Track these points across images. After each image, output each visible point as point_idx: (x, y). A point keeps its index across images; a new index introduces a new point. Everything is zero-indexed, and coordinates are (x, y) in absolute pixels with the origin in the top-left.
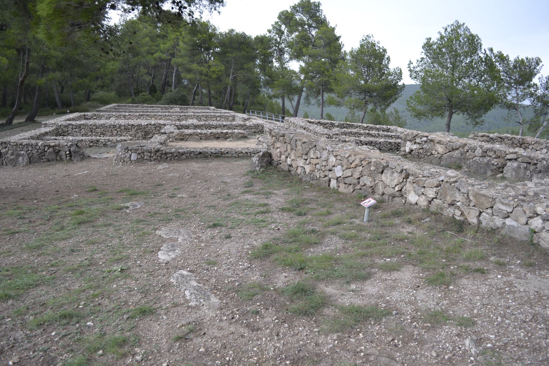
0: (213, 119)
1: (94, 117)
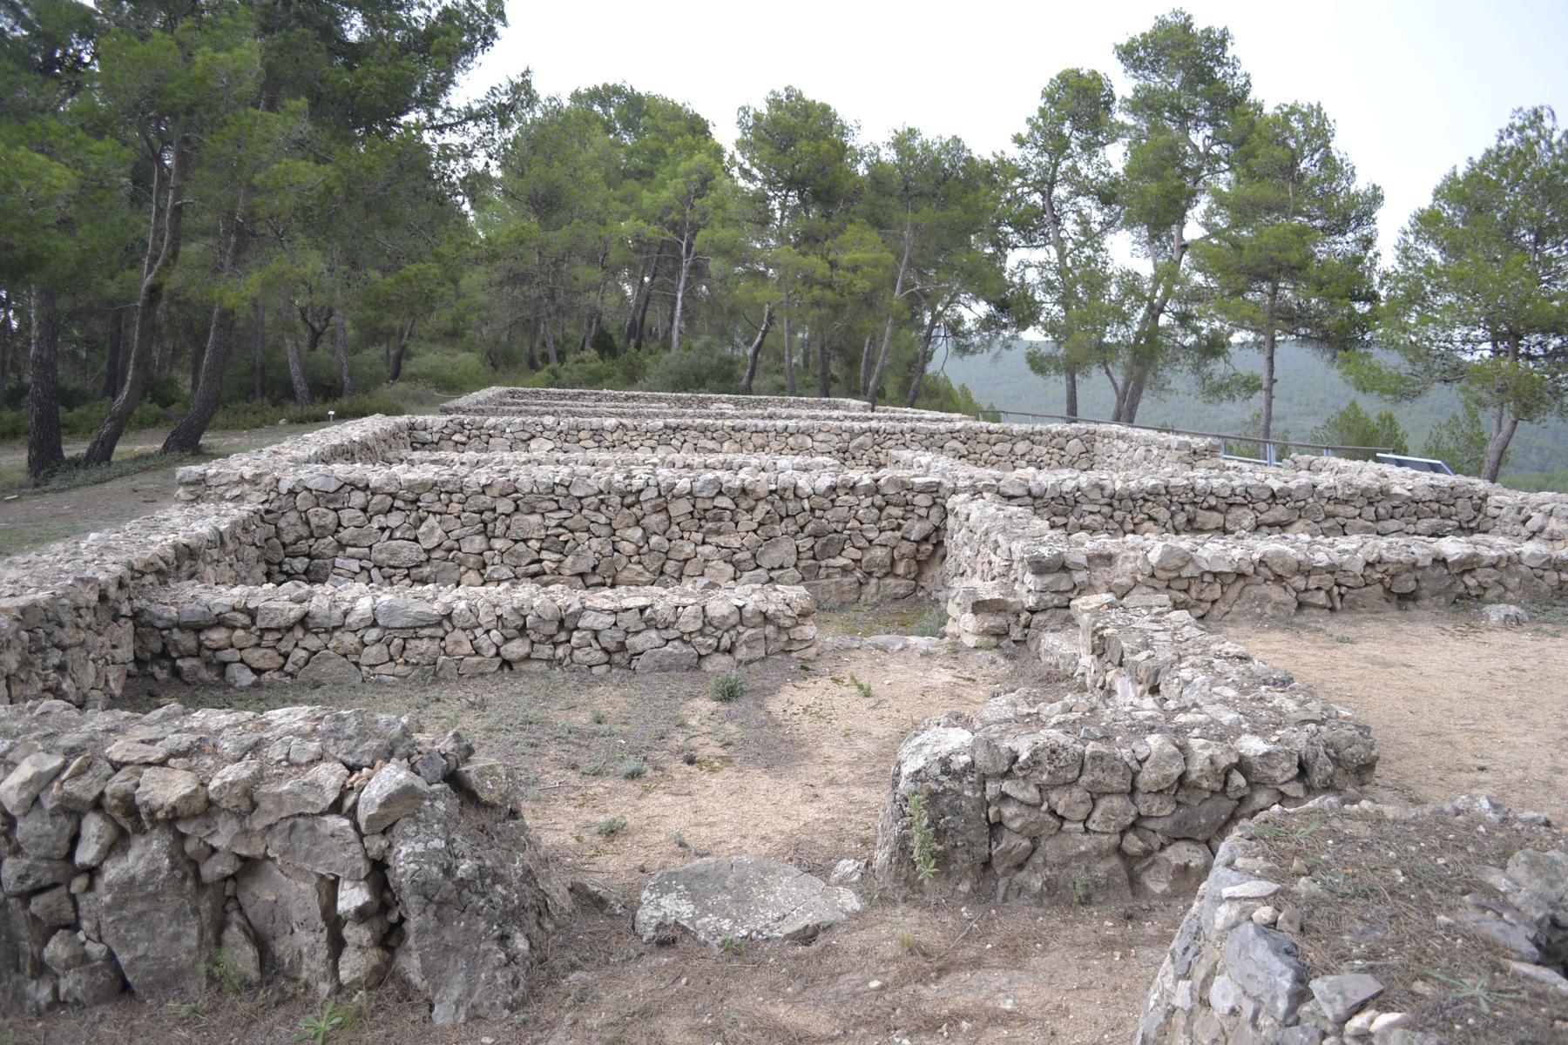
0: (997, 449)
1: (456, 437)
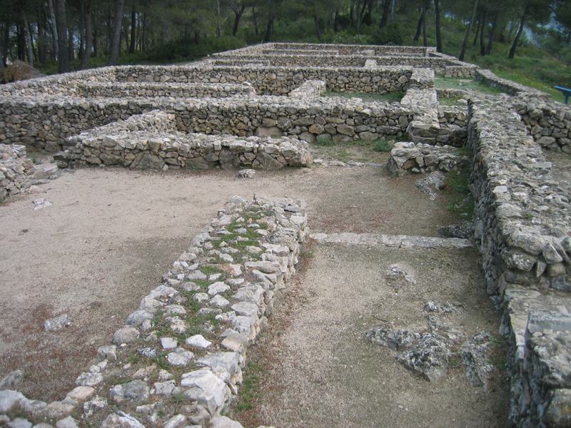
0: (363, 80)
1: (134, 75)
